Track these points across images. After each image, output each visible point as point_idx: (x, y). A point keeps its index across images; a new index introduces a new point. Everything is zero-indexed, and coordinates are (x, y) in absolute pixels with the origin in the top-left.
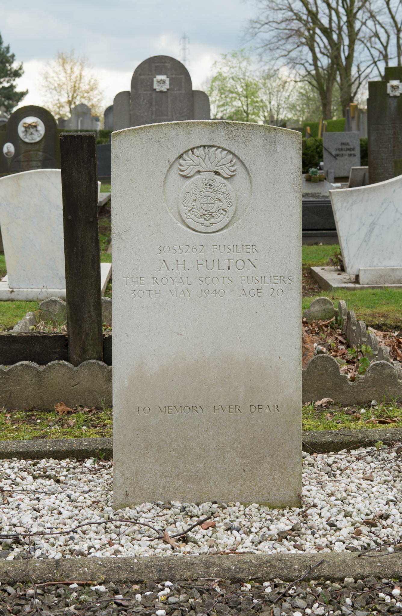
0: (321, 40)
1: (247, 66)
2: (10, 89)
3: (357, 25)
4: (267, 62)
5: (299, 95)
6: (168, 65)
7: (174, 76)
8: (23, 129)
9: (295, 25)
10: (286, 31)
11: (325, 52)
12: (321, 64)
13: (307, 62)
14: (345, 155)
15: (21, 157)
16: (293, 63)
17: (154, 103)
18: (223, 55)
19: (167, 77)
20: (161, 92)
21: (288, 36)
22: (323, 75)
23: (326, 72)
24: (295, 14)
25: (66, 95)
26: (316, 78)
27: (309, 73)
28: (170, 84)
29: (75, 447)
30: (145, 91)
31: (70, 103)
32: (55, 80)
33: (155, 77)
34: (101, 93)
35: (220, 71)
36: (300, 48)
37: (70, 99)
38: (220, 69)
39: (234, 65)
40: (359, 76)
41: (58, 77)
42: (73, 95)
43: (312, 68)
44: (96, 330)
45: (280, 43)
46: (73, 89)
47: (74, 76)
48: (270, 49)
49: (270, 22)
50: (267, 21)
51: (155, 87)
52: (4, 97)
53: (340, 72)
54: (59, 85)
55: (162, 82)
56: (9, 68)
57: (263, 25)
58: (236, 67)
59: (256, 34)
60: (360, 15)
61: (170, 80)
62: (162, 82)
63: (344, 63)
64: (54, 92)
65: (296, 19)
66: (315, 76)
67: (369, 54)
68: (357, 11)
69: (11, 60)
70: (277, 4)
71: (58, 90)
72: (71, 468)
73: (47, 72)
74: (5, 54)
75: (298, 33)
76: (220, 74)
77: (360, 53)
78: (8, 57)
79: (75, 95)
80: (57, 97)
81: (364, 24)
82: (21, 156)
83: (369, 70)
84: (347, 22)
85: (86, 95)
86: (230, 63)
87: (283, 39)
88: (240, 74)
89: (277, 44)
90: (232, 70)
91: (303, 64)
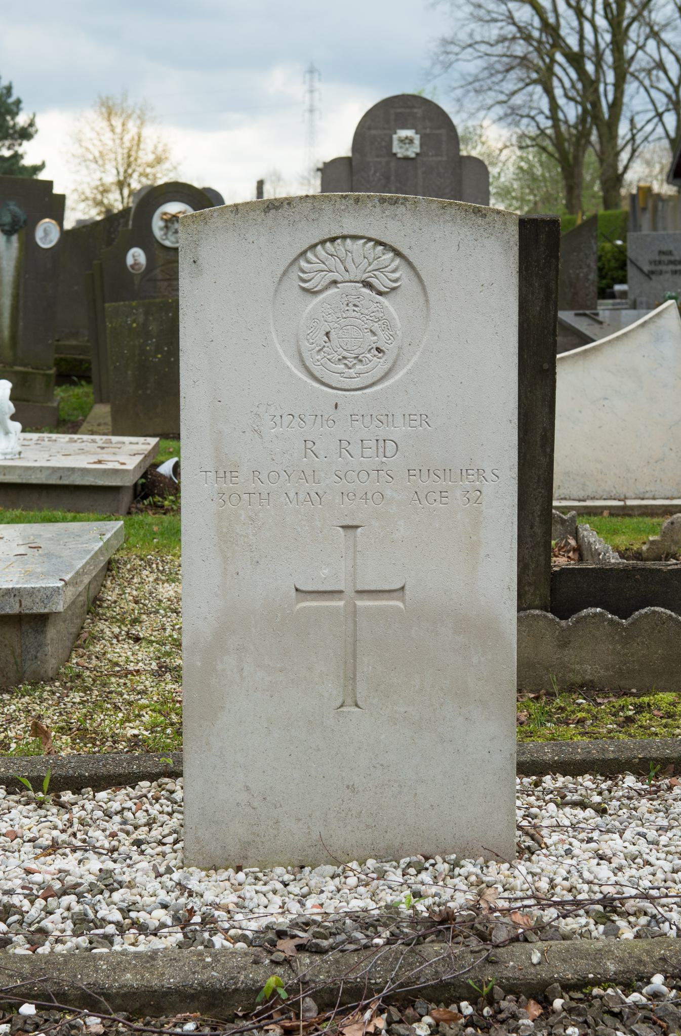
0: (565, 74)
2: (14, 161)
4: (473, 114)
5: (517, 171)
6: (419, 112)
7: (428, 131)
8: (161, 224)
9: (520, 48)
10: (505, 59)
11: (572, 93)
12: (565, 116)
13: (542, 112)
14: (666, 272)
15: (158, 273)
16: (513, 115)
17: (393, 178)
19: (417, 133)
20: (406, 158)
21: (508, 67)
22: (566, 136)
23: (574, 131)
24: (520, 29)
25: (115, 172)
26: (555, 141)
27: (543, 132)
28: (421, 145)
29: (595, 755)
30: (377, 156)
31: (121, 184)
32: (94, 145)
33: (395, 133)
34: (175, 168)
36: (530, 88)
37: (122, 178)
41: (100, 140)
42: (126, 171)
43: (549, 123)
44: (542, 558)
45: (495, 79)
46: (126, 161)
47: (127, 138)
48: (476, 91)
50: (469, 42)
51: (394, 151)
53: (598, 129)
54: (101, 153)
55: (406, 141)
56: (11, 123)
57: (464, 48)
59: (450, 65)
60: (633, 33)
61: (421, 138)
62: (407, 141)
63: (606, 116)
64: (93, 166)
65: (521, 38)
66: (553, 136)
67: (648, 99)
68: (630, 25)
69: (15, 109)
70: (489, 12)
71: (100, 162)
72: (604, 790)
73: (80, 131)
75: (524, 61)
77: (632, 97)
78: (9, 105)
79: (130, 171)
80: (98, 175)
81: (640, 48)
82: (158, 271)
83: (649, 128)
84: (612, 43)
85: (148, 170)
87: (498, 72)
89: (489, 81)
91: (533, 118)
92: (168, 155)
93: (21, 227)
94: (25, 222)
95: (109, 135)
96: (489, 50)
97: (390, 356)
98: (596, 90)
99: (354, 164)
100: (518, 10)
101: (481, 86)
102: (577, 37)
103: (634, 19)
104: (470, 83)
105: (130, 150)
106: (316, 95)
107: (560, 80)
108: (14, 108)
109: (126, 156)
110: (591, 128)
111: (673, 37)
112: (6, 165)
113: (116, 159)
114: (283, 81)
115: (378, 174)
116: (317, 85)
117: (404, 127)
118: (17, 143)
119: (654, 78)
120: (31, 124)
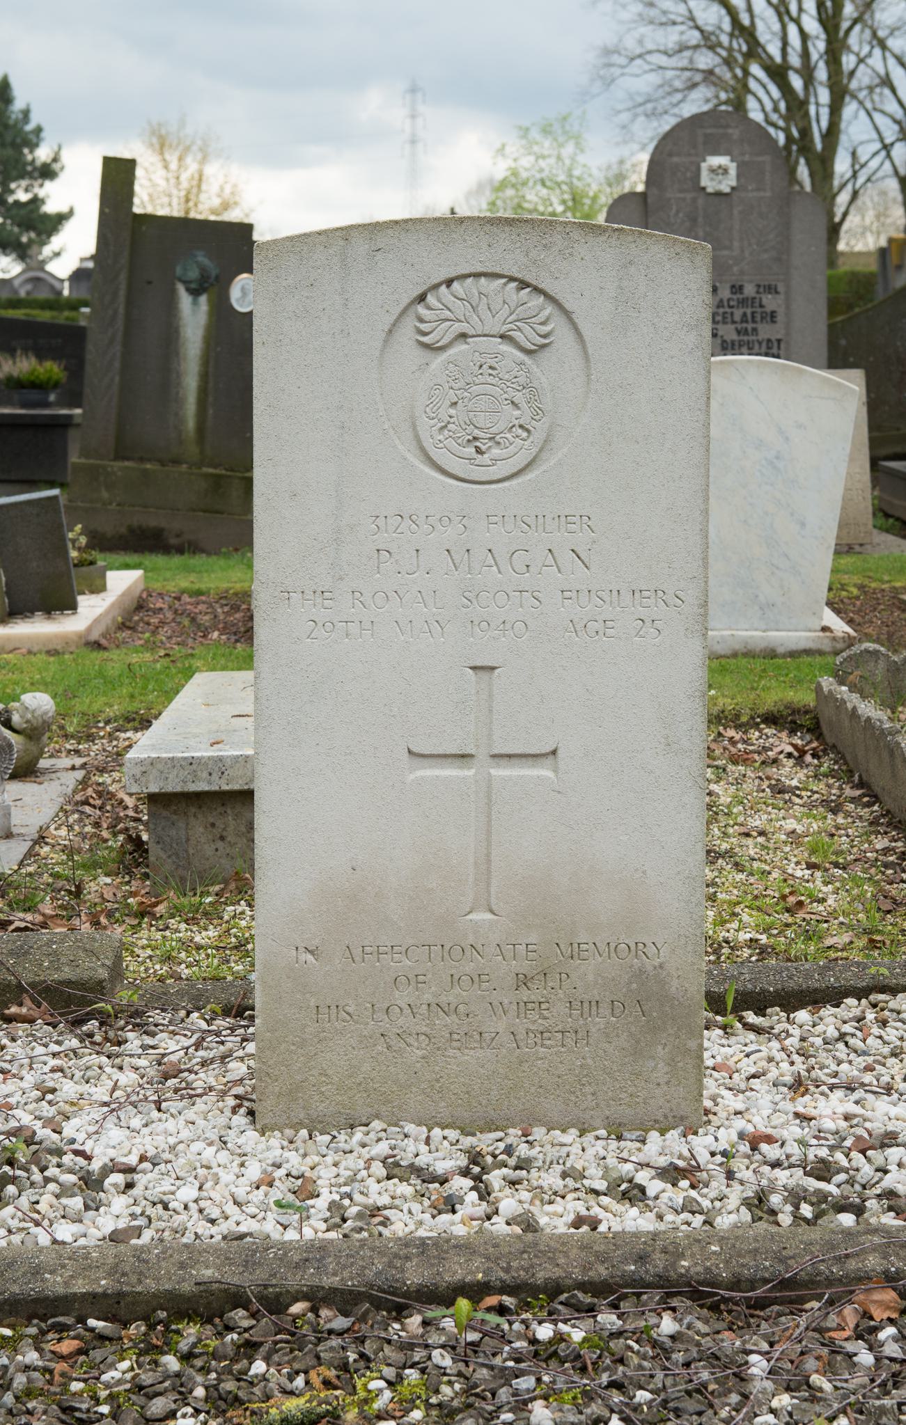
1: (575, 154)
2: (31, 207)
3: (848, 61)
7: (747, 158)
9: (705, 60)
17: (700, 220)
18: (520, 128)
19: (732, 161)
20: (719, 194)
28: (739, 176)
30: (681, 191)
33: (704, 160)
35: (513, 165)
38: (515, 160)
39: (546, 153)
40: (855, 175)
41: (150, 180)
47: (185, 177)
48: (647, 116)
49: (650, 52)
50: (638, 51)
51: (703, 184)
52: (19, 226)
54: (150, 196)
56: (29, 158)
57: (632, 59)
58: (549, 156)
59: (613, 80)
60: (853, 40)
61: (738, 167)
69: (35, 140)
70: (664, 13)
74: (19, 126)
76: (515, 173)
77: (849, 123)
78: (27, 133)
83: (874, 164)
84: (826, 52)
86: (536, 148)
87: (677, 90)
88: (560, 172)
89: (665, 102)
90: (542, 163)
92: (237, 198)
93: (212, 285)
94: (217, 277)
95: (162, 172)
96: (663, 60)
97: (538, 436)
98: (807, 114)
99: (649, 200)
100: (704, 10)
101: (655, 109)
102: (779, 44)
103: (855, 22)
104: (640, 105)
105: (189, 193)
106: (420, 121)
107: (760, 101)
108: (33, 138)
109: (183, 200)
110: (797, 162)
111: (897, 44)
112: (23, 212)
113: (170, 205)
114: (378, 105)
115: (681, 215)
116: (421, 108)
117: (716, 152)
118: (36, 184)
119: (876, 98)
120: (56, 159)
